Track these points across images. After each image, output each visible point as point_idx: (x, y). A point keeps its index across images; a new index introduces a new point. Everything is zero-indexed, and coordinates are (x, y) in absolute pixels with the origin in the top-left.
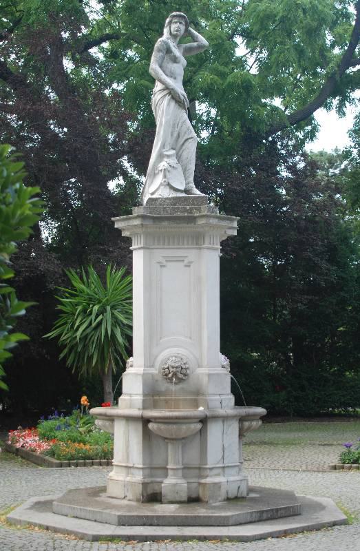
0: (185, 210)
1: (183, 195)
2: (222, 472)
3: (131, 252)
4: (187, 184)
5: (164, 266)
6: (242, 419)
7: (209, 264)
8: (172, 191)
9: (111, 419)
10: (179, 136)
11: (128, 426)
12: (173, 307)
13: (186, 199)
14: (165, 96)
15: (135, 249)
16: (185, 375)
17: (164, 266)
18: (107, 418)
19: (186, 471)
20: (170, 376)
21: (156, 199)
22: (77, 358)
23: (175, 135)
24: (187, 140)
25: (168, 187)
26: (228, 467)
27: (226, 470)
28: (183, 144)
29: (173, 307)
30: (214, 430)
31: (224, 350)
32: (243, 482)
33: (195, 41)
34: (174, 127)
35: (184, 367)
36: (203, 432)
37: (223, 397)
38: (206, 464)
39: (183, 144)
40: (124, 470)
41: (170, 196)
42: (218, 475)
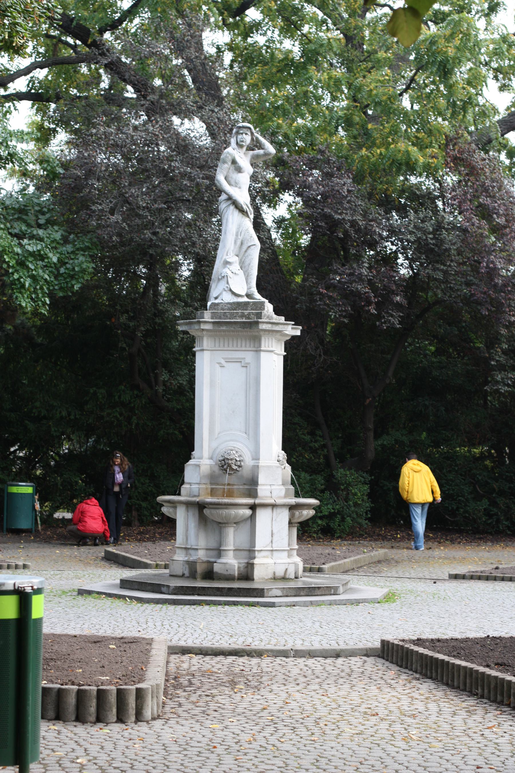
0: (243, 316)
1: (245, 299)
2: (270, 556)
3: (194, 355)
4: (249, 288)
5: (223, 366)
6: (292, 508)
7: (272, 365)
8: (233, 296)
9: (174, 504)
10: (242, 244)
11: (188, 511)
12: (240, 401)
13: (246, 304)
14: (229, 205)
15: (198, 351)
16: (240, 466)
17: (223, 366)
18: (172, 505)
19: (237, 552)
20: (225, 467)
21: (218, 304)
22: (409, 658)
23: (239, 243)
24: (249, 247)
25: (230, 293)
26: (276, 550)
27: (274, 553)
28: (246, 251)
29: (240, 401)
30: (263, 517)
31: (283, 449)
32: (291, 565)
33: (263, 149)
34: (237, 235)
35: (238, 459)
36: (253, 517)
37: (273, 487)
38: (255, 547)
39: (246, 251)
40: (184, 551)
41: (231, 301)
42: (267, 557)
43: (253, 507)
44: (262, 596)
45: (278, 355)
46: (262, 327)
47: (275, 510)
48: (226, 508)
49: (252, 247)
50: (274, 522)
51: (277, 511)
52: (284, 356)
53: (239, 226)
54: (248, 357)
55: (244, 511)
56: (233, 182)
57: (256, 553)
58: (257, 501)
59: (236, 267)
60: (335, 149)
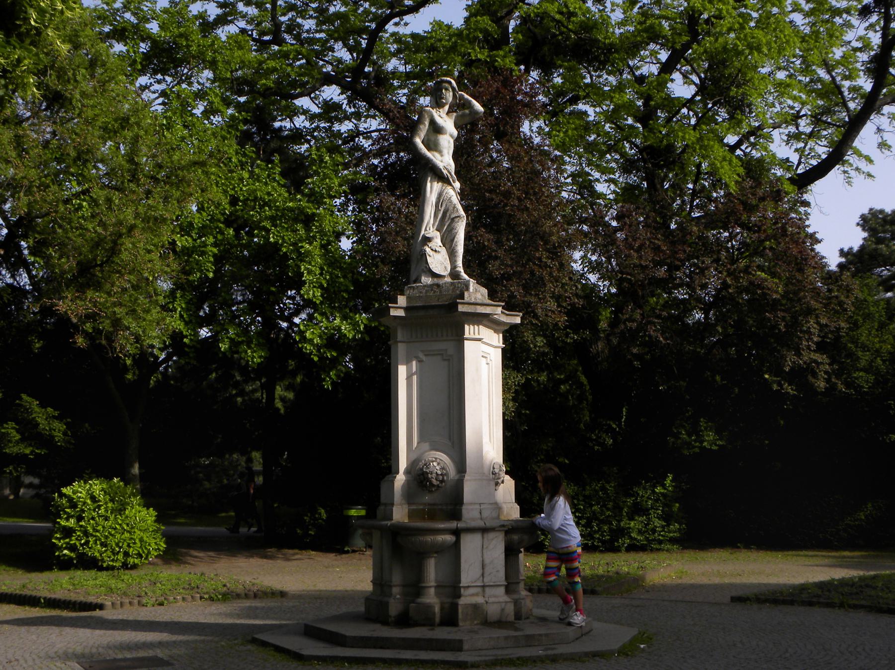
27: (487, 589)
36: (457, 545)
42: (477, 595)
43: (457, 533)
44: (460, 649)
45: (496, 347)
46: (461, 308)
47: (485, 535)
48: (434, 535)
49: (456, 220)
50: (485, 551)
51: (491, 535)
52: (503, 350)
53: (440, 195)
54: (449, 346)
55: (443, 537)
56: (432, 146)
57: (462, 590)
58: (461, 525)
59: (437, 242)
60: (722, 379)
